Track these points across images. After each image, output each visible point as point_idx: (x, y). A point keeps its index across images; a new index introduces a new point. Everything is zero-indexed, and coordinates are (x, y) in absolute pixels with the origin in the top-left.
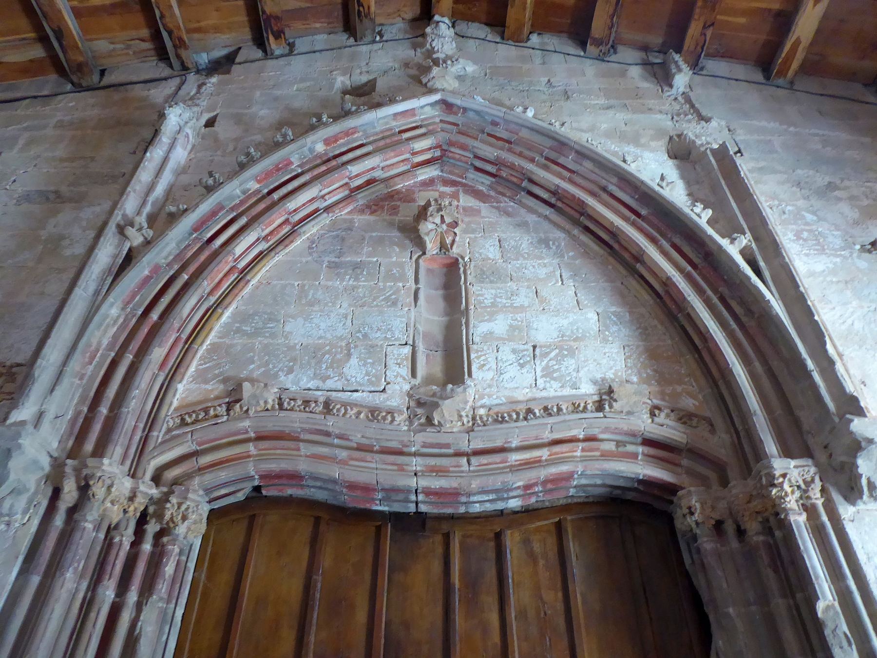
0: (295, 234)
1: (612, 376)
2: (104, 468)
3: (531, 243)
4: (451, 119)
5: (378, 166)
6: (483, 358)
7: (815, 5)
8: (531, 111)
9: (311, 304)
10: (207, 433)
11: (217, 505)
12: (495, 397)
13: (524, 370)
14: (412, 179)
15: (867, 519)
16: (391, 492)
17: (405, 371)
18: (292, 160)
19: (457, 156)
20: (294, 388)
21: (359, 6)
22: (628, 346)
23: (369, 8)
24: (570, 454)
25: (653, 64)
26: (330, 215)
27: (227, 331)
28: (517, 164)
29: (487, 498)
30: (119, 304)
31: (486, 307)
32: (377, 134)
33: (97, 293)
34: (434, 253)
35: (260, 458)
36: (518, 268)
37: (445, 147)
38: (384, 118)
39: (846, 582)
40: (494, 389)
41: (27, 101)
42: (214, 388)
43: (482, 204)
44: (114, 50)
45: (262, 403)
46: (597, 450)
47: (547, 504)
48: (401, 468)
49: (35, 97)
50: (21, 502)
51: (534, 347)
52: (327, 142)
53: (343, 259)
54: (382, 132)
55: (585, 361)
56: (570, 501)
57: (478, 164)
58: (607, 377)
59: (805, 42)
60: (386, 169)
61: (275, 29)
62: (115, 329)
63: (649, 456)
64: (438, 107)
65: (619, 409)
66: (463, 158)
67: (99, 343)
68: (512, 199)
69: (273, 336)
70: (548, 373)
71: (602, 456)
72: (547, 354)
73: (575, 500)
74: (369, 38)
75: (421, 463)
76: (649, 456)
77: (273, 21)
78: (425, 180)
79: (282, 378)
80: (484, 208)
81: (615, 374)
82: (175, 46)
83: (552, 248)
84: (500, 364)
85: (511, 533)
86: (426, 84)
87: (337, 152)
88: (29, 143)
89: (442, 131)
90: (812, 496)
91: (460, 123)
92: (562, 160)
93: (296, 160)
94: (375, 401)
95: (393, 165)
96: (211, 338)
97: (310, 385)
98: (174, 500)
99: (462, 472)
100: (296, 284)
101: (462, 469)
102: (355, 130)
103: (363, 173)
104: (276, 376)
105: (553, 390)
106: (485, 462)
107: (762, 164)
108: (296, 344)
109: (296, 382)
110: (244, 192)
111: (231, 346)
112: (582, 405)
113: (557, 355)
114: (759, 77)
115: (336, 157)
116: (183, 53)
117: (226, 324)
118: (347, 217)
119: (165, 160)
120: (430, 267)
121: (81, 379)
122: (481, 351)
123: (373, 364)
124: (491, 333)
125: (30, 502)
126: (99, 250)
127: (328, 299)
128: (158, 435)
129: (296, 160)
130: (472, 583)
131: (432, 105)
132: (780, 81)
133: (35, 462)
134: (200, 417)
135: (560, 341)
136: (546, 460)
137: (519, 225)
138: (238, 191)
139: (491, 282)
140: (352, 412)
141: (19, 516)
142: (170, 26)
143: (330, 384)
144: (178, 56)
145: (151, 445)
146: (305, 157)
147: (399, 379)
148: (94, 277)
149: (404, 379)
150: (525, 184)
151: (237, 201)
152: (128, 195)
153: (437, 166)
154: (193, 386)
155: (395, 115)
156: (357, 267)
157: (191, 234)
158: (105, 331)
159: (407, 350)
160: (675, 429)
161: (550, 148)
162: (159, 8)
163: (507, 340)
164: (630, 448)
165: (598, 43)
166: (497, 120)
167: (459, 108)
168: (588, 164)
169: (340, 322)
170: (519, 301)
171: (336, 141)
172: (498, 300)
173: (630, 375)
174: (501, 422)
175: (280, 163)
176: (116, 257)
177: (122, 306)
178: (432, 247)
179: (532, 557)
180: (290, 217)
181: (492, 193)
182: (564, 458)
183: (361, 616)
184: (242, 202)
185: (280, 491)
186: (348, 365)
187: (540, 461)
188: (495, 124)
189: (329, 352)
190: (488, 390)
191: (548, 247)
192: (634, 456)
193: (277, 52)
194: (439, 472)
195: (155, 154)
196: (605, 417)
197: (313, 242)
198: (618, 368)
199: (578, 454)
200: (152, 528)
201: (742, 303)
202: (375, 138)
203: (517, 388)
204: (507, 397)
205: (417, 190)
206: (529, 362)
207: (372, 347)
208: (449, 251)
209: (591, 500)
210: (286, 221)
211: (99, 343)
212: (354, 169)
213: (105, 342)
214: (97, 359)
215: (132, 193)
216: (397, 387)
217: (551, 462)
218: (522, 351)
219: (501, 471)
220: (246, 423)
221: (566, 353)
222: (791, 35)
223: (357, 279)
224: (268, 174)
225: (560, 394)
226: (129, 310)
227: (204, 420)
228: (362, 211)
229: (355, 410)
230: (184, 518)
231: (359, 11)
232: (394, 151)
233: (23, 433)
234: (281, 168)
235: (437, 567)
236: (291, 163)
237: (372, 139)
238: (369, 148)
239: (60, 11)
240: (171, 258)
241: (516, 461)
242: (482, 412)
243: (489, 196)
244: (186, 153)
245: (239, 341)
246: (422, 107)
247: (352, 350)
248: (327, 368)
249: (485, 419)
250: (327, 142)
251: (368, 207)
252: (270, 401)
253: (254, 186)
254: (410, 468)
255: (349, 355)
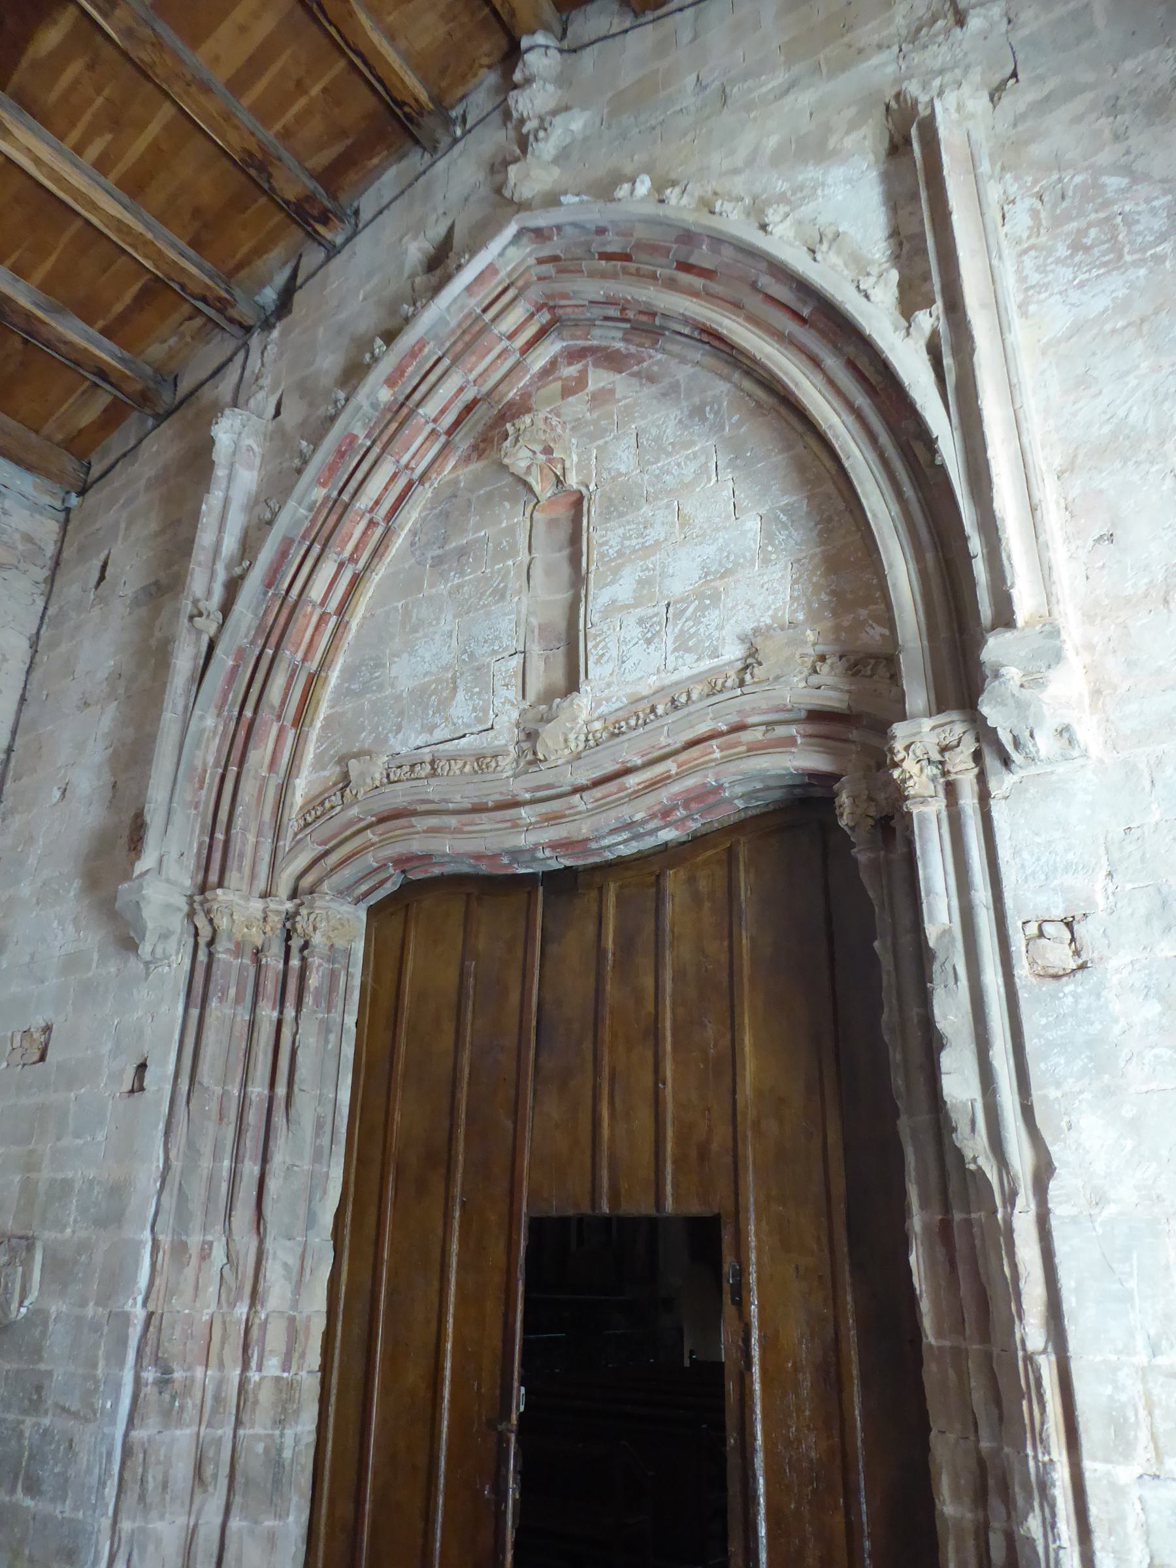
0: (390, 532)
1: (769, 621)
2: (220, 898)
3: (680, 421)
5: (468, 382)
6: (601, 646)
8: (643, 182)
9: (415, 630)
10: (325, 829)
11: (373, 899)
12: (614, 699)
13: (652, 647)
14: (524, 375)
15: (1032, 790)
17: (513, 693)
18: (355, 432)
20: (404, 751)
21: (401, 108)
23: (416, 100)
24: (706, 758)
26: (427, 485)
27: (342, 693)
29: (620, 839)
30: (213, 711)
31: (612, 560)
32: (453, 332)
33: (186, 707)
34: (549, 495)
35: (384, 842)
36: (657, 476)
38: (455, 301)
39: (969, 894)
40: (614, 688)
41: (120, 464)
42: (332, 772)
43: (618, 376)
44: (170, 348)
45: (369, 781)
46: (740, 744)
47: (716, 825)
48: (515, 824)
49: (124, 455)
50: (172, 944)
51: (669, 605)
52: (390, 382)
53: (447, 548)
54: (459, 325)
55: (733, 608)
56: (743, 815)
58: (762, 624)
60: (480, 381)
61: (315, 213)
62: (217, 740)
63: (810, 736)
64: (525, 240)
65: (763, 677)
67: (205, 764)
68: (653, 346)
70: (682, 645)
71: (749, 750)
72: (683, 611)
73: (750, 813)
74: (445, 141)
76: (810, 736)
77: (307, 207)
78: (545, 366)
79: (392, 741)
80: (618, 382)
81: (773, 617)
82: (219, 311)
83: (706, 419)
85: (675, 873)
87: (409, 389)
88: (130, 524)
89: (540, 279)
90: (953, 770)
91: (558, 252)
93: (360, 432)
95: (486, 370)
96: (323, 710)
97: (419, 743)
98: (304, 911)
99: (580, 813)
100: (400, 605)
101: (579, 809)
102: (421, 344)
103: (450, 402)
104: (386, 739)
105: (688, 667)
106: (599, 795)
107: (1052, 83)
108: (402, 691)
109: (404, 743)
110: (310, 509)
111: (343, 714)
112: (720, 682)
113: (695, 610)
115: (408, 397)
116: (232, 312)
117: (336, 687)
118: (453, 476)
119: (226, 501)
120: (554, 516)
121: (196, 808)
122: (599, 635)
123: (479, 693)
124: (614, 602)
125: (179, 942)
126: (177, 658)
127: (432, 616)
128: (286, 843)
129: (360, 432)
130: (626, 944)
133: (168, 906)
134: (319, 813)
135: (701, 586)
136: (677, 774)
137: (664, 395)
138: (303, 511)
140: (456, 767)
141: (174, 957)
142: (198, 291)
143: (438, 735)
144: (231, 320)
145: (280, 856)
146: (370, 420)
147: (508, 706)
148: (180, 691)
149: (513, 704)
151: (307, 523)
152: (192, 575)
153: (553, 336)
154: (314, 776)
155: (469, 289)
156: (462, 552)
157: (266, 593)
158: (207, 747)
159: (516, 661)
162: (173, 280)
164: (781, 731)
167: (551, 228)
170: (653, 535)
171: (403, 372)
172: (627, 543)
173: (796, 611)
174: (617, 735)
175: (340, 446)
176: (196, 657)
177: (216, 712)
178: (543, 488)
179: (697, 898)
180: (373, 515)
182: (698, 765)
183: (514, 997)
184: (313, 521)
185: (426, 872)
186: (454, 703)
187: (669, 777)
188: (601, 231)
189: (434, 692)
190: (606, 691)
191: (703, 419)
192: (790, 741)
193: (339, 240)
194: (553, 819)
195: (214, 498)
197: (415, 535)
200: (296, 943)
202: (452, 340)
204: (627, 696)
206: (658, 632)
207: (478, 669)
209: (771, 807)
210: (372, 523)
211: (205, 764)
212: (430, 409)
213: (211, 760)
214: (207, 781)
215: (197, 569)
216: (505, 718)
217: (680, 776)
218: (651, 618)
219: (619, 803)
220: (354, 811)
221: (708, 602)
223: (462, 573)
224: (332, 468)
225: (695, 671)
226: (225, 713)
227: (323, 814)
228: (467, 460)
229: (460, 764)
230: (315, 929)
231: (405, 114)
232: (474, 353)
233: (145, 884)
234: (346, 451)
235: (591, 929)
236: (355, 437)
237: (448, 344)
238: (446, 362)
239: (86, 350)
240: (253, 632)
241: (639, 784)
242: (598, 725)
244: (255, 473)
245: (349, 705)
246: (502, 254)
249: (598, 735)
250: (390, 382)
251: (475, 447)
252: (377, 776)
253: (319, 493)
254: (523, 822)
255: (455, 689)
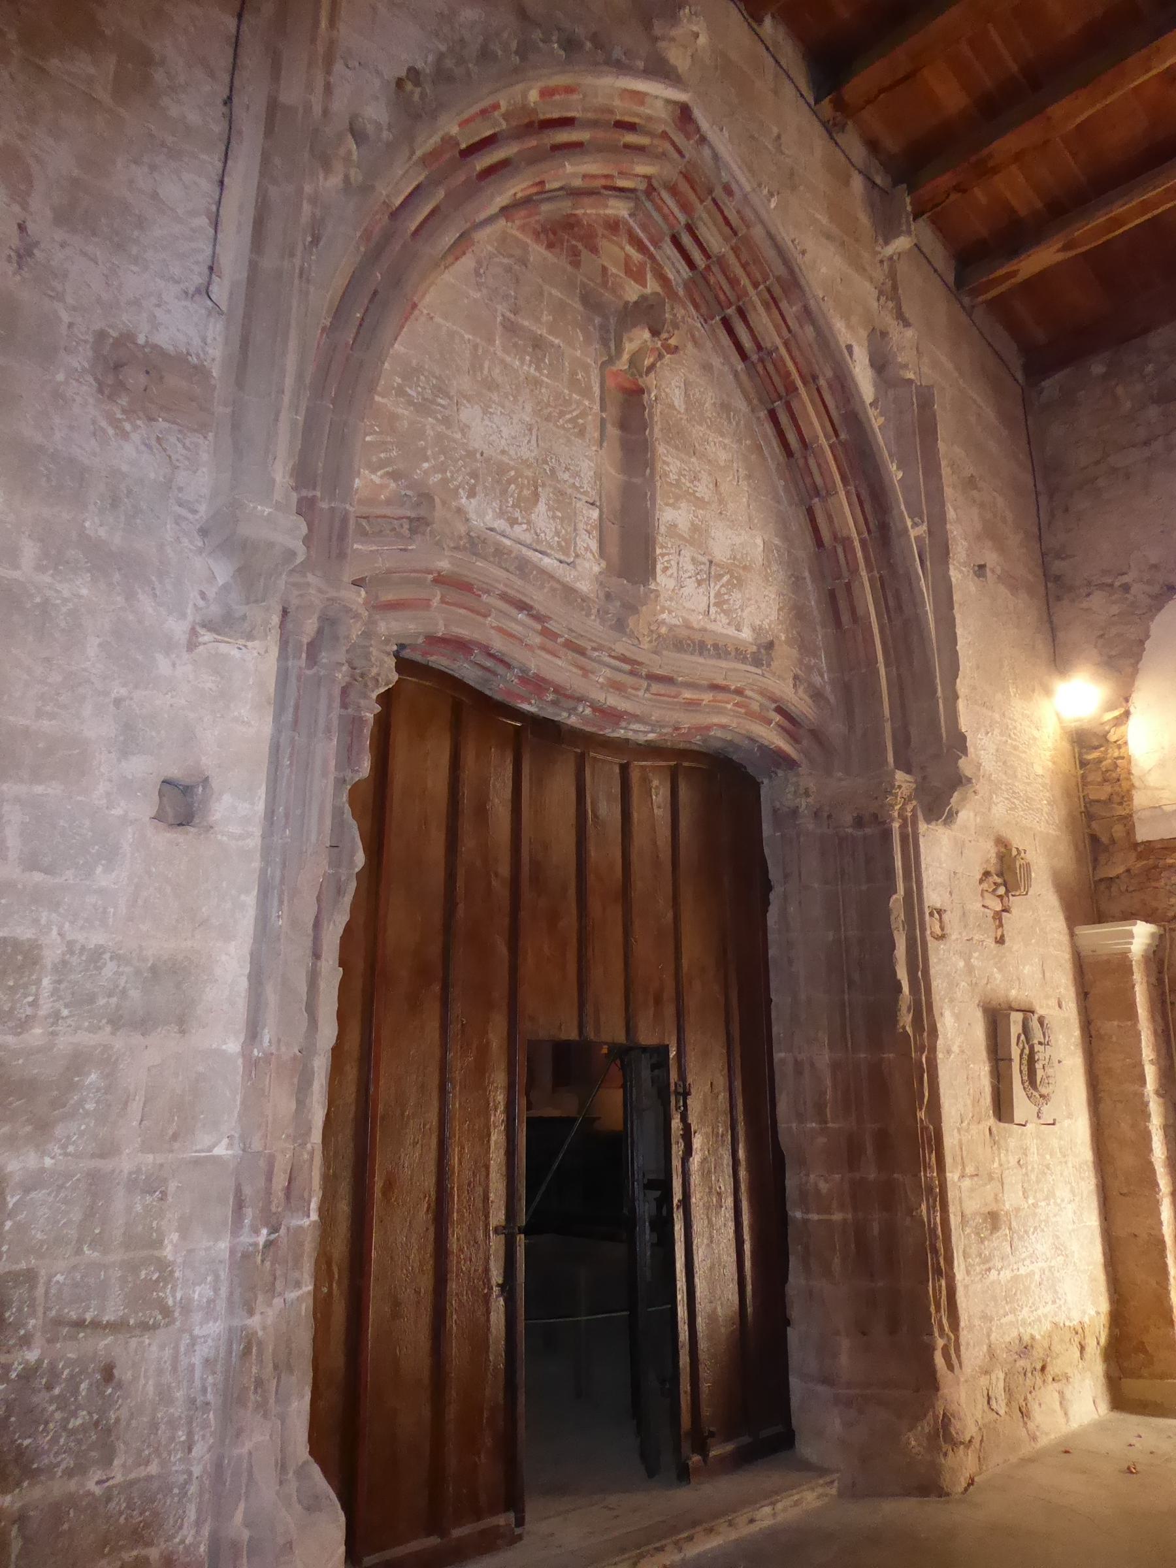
4: (679, 139)
7: (1059, 251)
16: (538, 684)
19: (666, 210)
22: (784, 595)
25: (874, 183)
28: (742, 283)
37: (655, 184)
57: (686, 240)
59: (1022, 276)
66: (671, 217)
69: (447, 421)
75: (609, 675)
84: (681, 573)
86: (655, 39)
91: (687, 156)
92: (784, 305)
94: (565, 576)
105: (720, 626)
114: (951, 279)
131: (668, 101)
132: (966, 300)
139: (676, 448)
150: (731, 311)
160: (810, 708)
161: (778, 279)
163: (687, 541)
165: (840, 105)
166: (734, 186)
167: (698, 129)
168: (809, 331)
169: (525, 435)
181: (681, 292)
188: (728, 191)
192: (769, 722)
196: (763, 675)
198: (773, 619)
199: (729, 706)
201: (897, 596)
203: (694, 611)
205: (600, 231)
208: (641, 376)
216: (587, 565)
222: (1015, 261)
243: (676, 294)
247: (540, 489)
248: (513, 506)
